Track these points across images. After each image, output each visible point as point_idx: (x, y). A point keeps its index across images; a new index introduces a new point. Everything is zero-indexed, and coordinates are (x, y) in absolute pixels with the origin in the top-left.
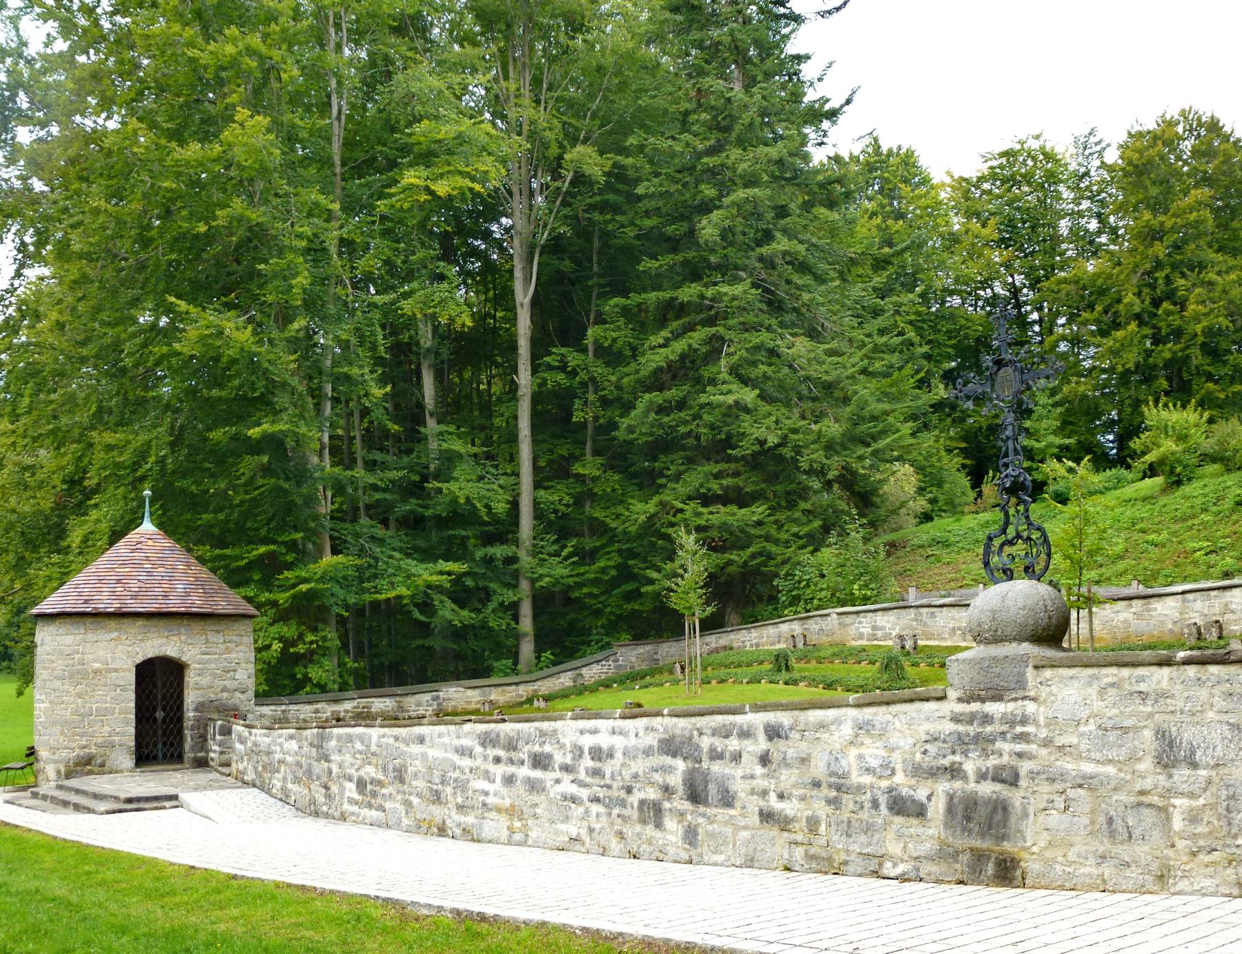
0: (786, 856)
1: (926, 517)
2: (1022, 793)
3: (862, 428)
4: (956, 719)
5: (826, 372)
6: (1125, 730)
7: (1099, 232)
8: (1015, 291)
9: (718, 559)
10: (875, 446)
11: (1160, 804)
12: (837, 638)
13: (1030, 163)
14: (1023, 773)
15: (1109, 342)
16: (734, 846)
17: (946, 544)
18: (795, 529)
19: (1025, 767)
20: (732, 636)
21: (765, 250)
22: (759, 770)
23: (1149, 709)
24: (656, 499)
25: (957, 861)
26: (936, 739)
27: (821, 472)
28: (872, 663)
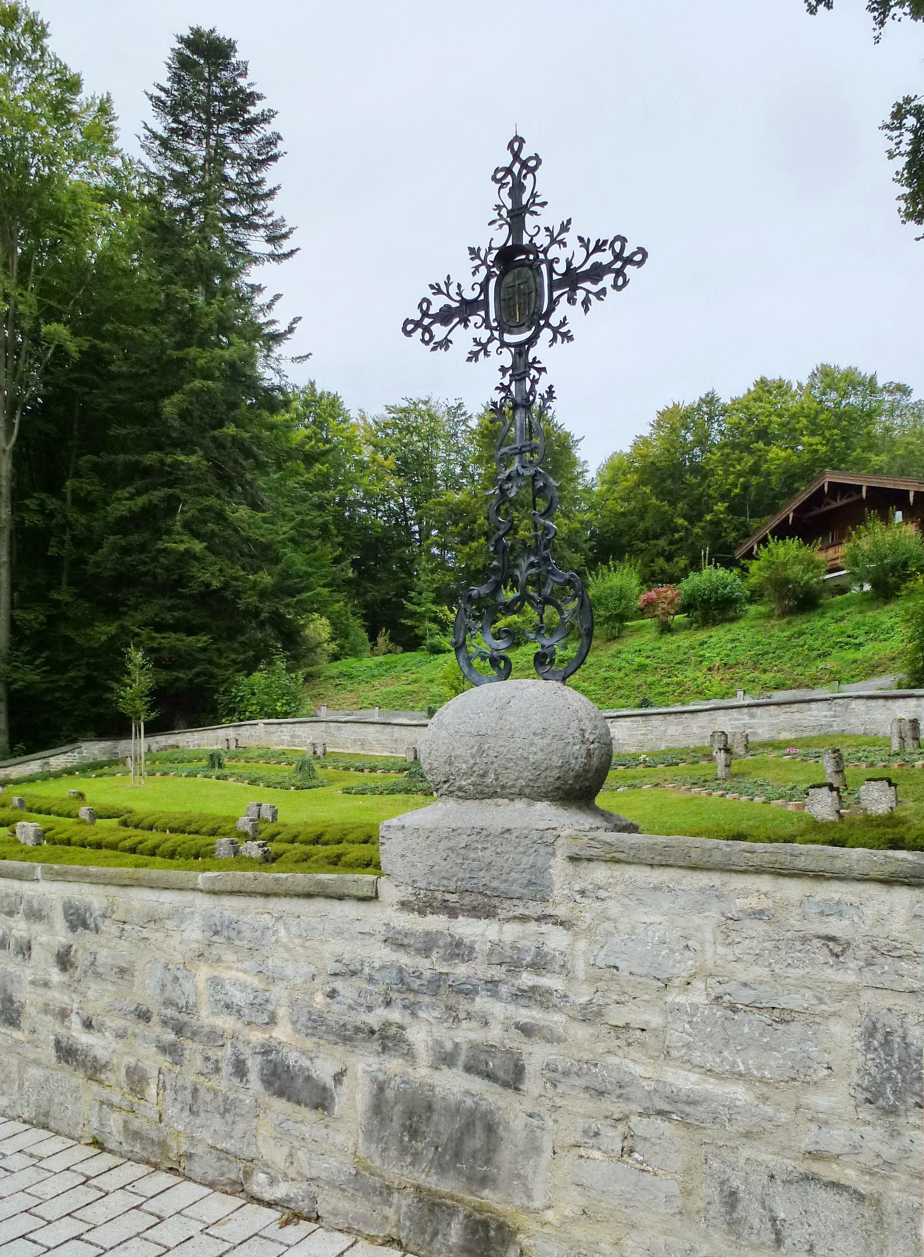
0: (95, 1123)
1: (335, 658)
2: (528, 1107)
3: (290, 582)
4: (395, 941)
5: (263, 536)
6: (784, 1017)
7: (462, 476)
8: (404, 509)
9: (164, 675)
10: (298, 597)
11: (863, 1189)
12: (263, 743)
13: (420, 420)
14: (533, 1066)
15: (466, 550)
16: (21, 1086)
17: (350, 677)
18: (234, 656)
19: (536, 1056)
20: (178, 737)
21: (216, 433)
22: (56, 976)
23: (850, 978)
24: (116, 624)
25: (387, 1202)
26: (354, 973)
27: (256, 614)
28: (290, 764)
